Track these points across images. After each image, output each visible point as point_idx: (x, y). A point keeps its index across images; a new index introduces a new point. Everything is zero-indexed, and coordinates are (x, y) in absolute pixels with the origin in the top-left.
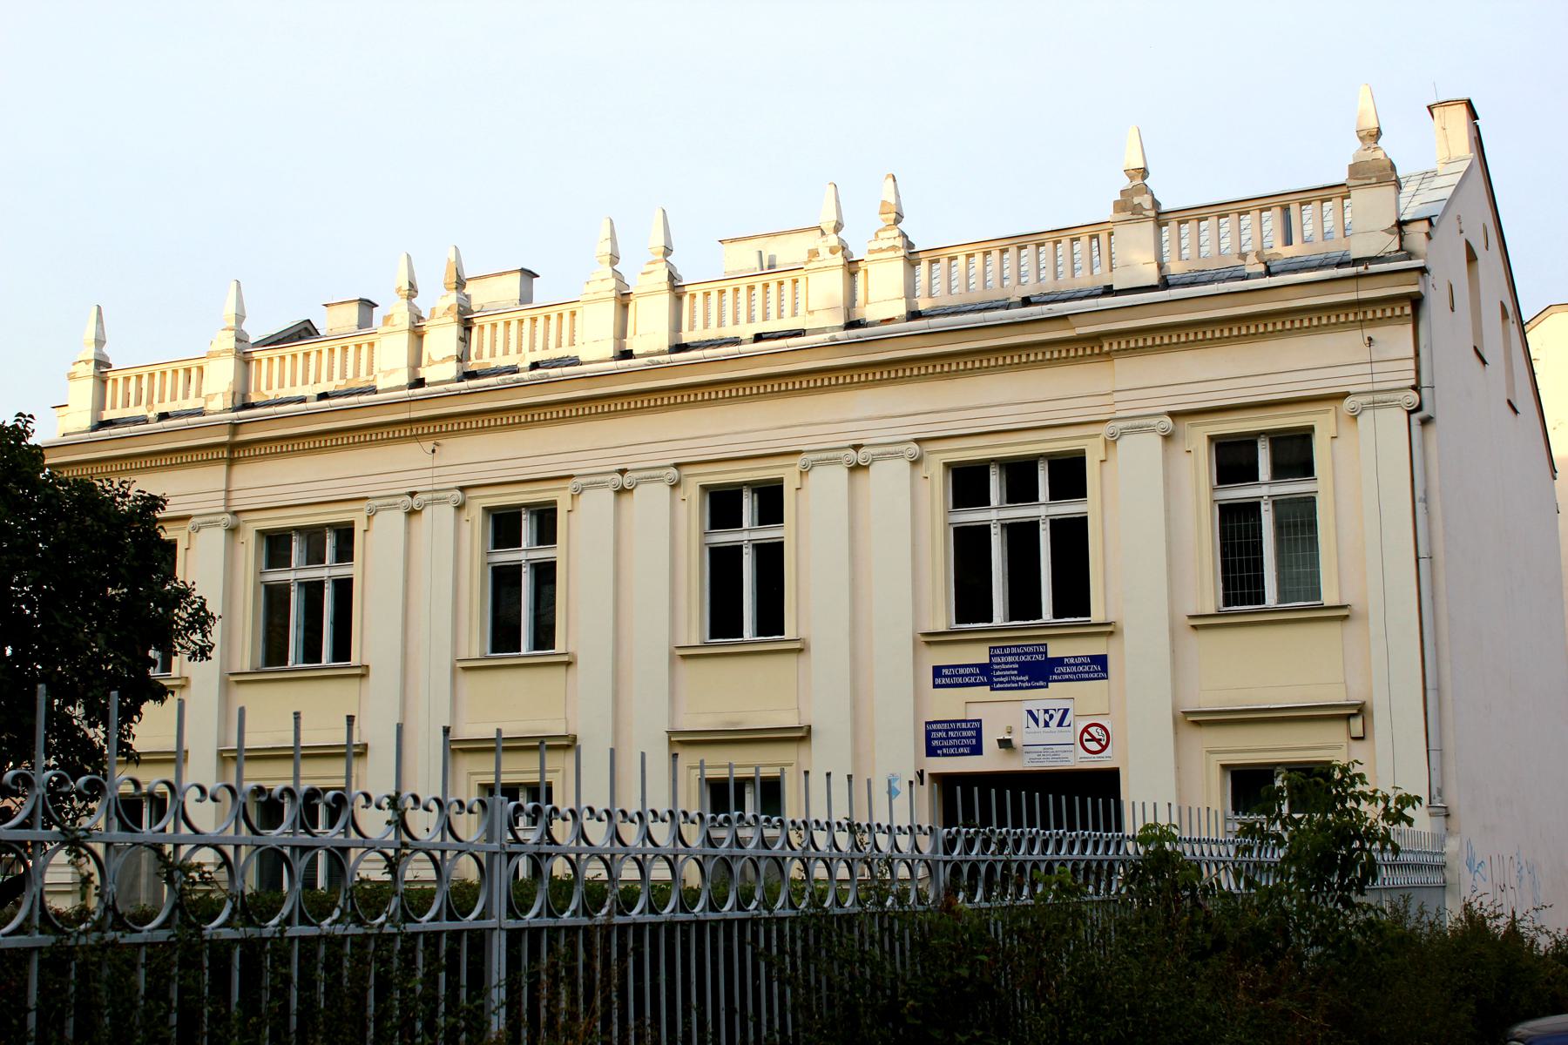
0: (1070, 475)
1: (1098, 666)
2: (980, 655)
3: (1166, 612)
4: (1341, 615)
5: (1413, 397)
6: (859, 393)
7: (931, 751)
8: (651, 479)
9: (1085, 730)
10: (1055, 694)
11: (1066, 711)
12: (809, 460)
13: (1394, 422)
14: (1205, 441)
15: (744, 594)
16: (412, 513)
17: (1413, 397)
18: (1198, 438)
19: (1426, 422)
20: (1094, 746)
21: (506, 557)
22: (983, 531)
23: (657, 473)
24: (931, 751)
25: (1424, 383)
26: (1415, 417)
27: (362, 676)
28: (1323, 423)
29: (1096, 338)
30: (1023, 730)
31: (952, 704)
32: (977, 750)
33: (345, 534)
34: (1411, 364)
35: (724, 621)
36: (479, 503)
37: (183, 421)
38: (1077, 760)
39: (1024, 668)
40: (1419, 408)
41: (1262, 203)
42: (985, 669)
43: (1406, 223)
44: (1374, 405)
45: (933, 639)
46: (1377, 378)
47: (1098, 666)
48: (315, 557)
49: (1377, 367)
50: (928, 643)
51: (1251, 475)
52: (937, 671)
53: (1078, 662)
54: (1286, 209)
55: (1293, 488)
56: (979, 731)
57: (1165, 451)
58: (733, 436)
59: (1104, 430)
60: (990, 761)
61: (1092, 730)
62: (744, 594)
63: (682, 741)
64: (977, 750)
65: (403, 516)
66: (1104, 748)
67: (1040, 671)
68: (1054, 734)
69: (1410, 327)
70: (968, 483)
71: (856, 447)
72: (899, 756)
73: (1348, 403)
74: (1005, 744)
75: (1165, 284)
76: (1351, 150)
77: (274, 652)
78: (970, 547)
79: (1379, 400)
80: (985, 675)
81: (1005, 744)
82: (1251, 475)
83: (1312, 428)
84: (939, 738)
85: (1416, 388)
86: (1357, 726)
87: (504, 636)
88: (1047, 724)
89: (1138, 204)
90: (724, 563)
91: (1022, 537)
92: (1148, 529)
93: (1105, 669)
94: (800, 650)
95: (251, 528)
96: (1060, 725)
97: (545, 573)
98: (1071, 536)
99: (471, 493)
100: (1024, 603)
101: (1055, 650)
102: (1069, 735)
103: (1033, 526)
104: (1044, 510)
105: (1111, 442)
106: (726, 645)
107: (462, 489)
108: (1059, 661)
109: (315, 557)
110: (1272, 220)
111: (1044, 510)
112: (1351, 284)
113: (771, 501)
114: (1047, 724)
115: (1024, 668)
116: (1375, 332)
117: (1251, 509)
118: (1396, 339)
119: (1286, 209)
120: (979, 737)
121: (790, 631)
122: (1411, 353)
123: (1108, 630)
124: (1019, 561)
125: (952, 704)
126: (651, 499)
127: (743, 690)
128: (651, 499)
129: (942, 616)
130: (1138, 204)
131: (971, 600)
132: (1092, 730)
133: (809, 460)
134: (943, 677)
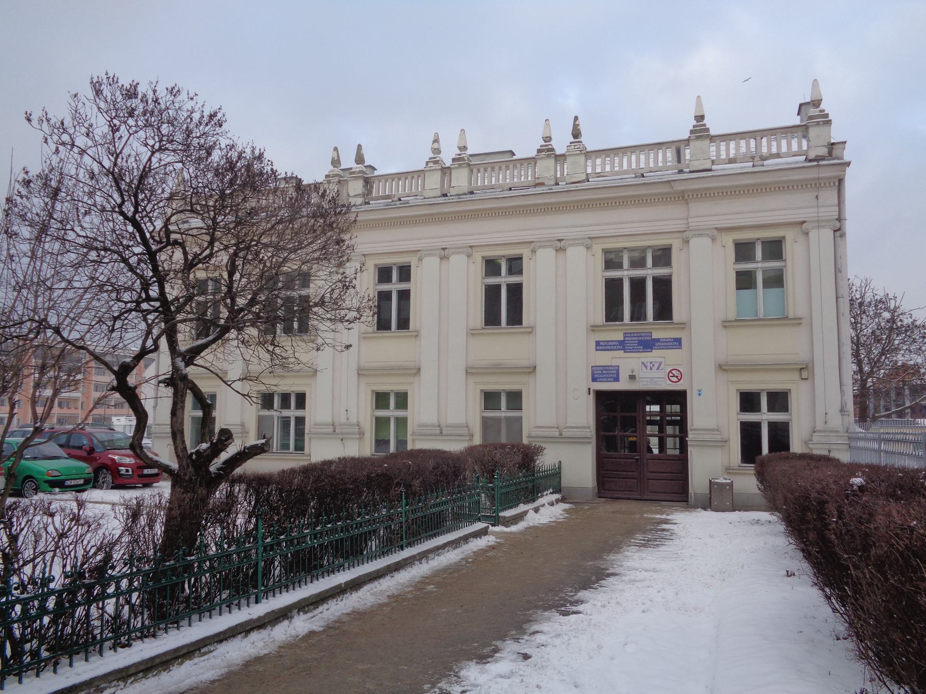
2: (619, 336)
3: (815, 377)
7: (594, 379)
8: (429, 255)
9: (670, 372)
10: (656, 355)
11: (661, 363)
12: (533, 246)
15: (504, 304)
16: (560, 250)
18: (728, 241)
20: (674, 379)
22: (620, 281)
24: (594, 379)
26: (838, 233)
28: (791, 237)
30: (641, 372)
31: (606, 358)
32: (617, 379)
34: (837, 209)
35: (492, 318)
38: (666, 385)
40: (839, 229)
43: (833, 144)
45: (594, 328)
46: (821, 214)
49: (820, 209)
52: (598, 343)
53: (667, 341)
56: (618, 371)
58: (500, 235)
60: (623, 385)
61: (674, 372)
62: (504, 304)
63: (722, 368)
64: (617, 379)
66: (679, 380)
67: (648, 344)
68: (655, 373)
69: (835, 193)
78: (613, 288)
80: (622, 345)
83: (784, 238)
88: (651, 369)
90: (492, 293)
91: (638, 285)
92: (703, 280)
93: (680, 344)
94: (530, 332)
96: (658, 369)
97: (404, 296)
99: (475, 249)
100: (638, 314)
101: (655, 335)
102: (663, 373)
106: (492, 330)
108: (658, 340)
111: (649, 272)
113: (405, 273)
114: (651, 369)
115: (640, 343)
120: (618, 374)
123: (683, 326)
124: (640, 297)
125: (606, 358)
127: (504, 346)
129: (599, 315)
131: (613, 312)
132: (674, 372)
133: (533, 246)
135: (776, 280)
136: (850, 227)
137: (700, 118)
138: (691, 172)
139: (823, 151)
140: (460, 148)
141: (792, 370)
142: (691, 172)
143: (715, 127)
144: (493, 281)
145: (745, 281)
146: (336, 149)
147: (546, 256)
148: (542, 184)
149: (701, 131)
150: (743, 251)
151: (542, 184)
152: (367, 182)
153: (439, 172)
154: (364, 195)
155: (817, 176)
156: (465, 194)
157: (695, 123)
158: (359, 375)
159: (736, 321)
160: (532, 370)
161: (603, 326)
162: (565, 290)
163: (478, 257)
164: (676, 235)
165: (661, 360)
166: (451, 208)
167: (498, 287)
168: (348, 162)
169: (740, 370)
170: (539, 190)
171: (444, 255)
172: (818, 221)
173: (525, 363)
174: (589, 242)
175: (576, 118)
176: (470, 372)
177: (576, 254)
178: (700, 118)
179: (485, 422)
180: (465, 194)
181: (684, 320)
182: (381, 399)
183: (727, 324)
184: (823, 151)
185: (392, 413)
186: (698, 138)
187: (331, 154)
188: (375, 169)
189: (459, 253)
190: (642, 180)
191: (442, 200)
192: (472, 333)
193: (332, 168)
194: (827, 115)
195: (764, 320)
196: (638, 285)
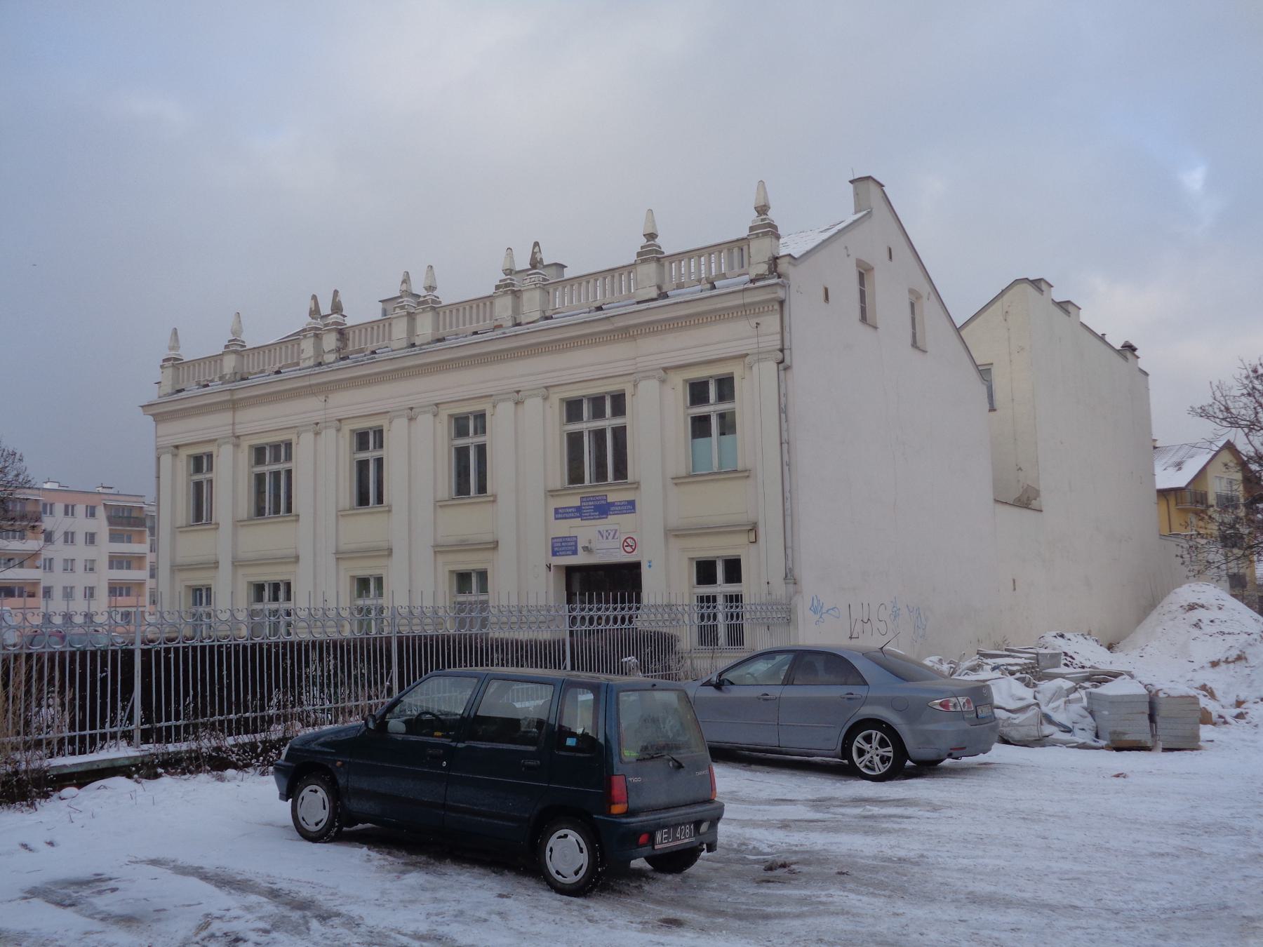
0: (619, 403)
1: (630, 506)
2: (575, 501)
5: (780, 355)
7: (554, 554)
8: (504, 400)
10: (612, 521)
13: (770, 367)
14: (681, 383)
15: (469, 474)
16: (317, 434)
17: (780, 355)
19: (786, 369)
20: (629, 549)
21: (575, 427)
24: (554, 554)
25: (787, 345)
26: (781, 366)
27: (494, 501)
29: (626, 329)
30: (600, 544)
31: (564, 528)
32: (575, 552)
33: (481, 417)
34: (778, 337)
36: (347, 428)
40: (782, 361)
41: (717, 248)
42: (579, 509)
44: (759, 360)
45: (552, 493)
47: (630, 506)
48: (598, 413)
49: (760, 339)
52: (556, 510)
56: (576, 542)
57: (409, 426)
58: (461, 387)
59: (631, 378)
60: (580, 559)
64: (575, 552)
65: (775, 366)
67: (603, 510)
69: (778, 317)
70: (573, 409)
71: (518, 392)
72: (539, 555)
73: (747, 360)
74: (586, 549)
76: (751, 217)
77: (260, 511)
78: (575, 441)
80: (579, 512)
81: (586, 549)
84: (562, 545)
85: (782, 350)
87: (462, 488)
91: (599, 435)
95: (245, 444)
99: (552, 390)
100: (600, 475)
101: (611, 498)
102: (617, 543)
103: (580, 434)
104: (609, 423)
106: (363, 510)
107: (546, 388)
108: (613, 504)
109: (277, 459)
112: (769, 290)
118: (771, 322)
120: (576, 545)
121: (630, 478)
124: (596, 452)
125: (564, 528)
126: (425, 420)
127: (469, 520)
130: (651, 253)
131: (575, 476)
134: (560, 514)
135: (728, 424)
136: (797, 358)
137: (651, 236)
138: (638, 303)
139: (763, 269)
140: (233, 333)
141: (740, 531)
142: (638, 303)
143: (668, 246)
144: (461, 442)
145: (700, 426)
146: (314, 297)
147: (506, 408)
148: (500, 326)
149: (650, 252)
150: (698, 392)
151: (500, 326)
152: (342, 334)
153: (405, 319)
154: (338, 350)
155: (741, 302)
156: (429, 343)
157: (644, 241)
158: (435, 552)
159: (689, 476)
160: (494, 546)
161: (565, 489)
162: (527, 449)
163: (556, 398)
164: (625, 378)
165: (616, 527)
166: (420, 361)
167: (580, 434)
168: (418, 288)
169: (690, 535)
170: (498, 333)
171: (412, 414)
172: (759, 353)
173: (489, 538)
175: (336, 292)
176: (340, 556)
177: (533, 405)
178: (651, 236)
179: (461, 607)
180: (429, 343)
182: (705, 571)
183: (678, 481)
184: (763, 269)
185: (721, 588)
186: (643, 261)
187: (309, 304)
188: (564, 267)
189: (425, 412)
190: (600, 314)
191: (317, 370)
192: (440, 505)
193: (310, 319)
194: (775, 227)
195: (719, 473)
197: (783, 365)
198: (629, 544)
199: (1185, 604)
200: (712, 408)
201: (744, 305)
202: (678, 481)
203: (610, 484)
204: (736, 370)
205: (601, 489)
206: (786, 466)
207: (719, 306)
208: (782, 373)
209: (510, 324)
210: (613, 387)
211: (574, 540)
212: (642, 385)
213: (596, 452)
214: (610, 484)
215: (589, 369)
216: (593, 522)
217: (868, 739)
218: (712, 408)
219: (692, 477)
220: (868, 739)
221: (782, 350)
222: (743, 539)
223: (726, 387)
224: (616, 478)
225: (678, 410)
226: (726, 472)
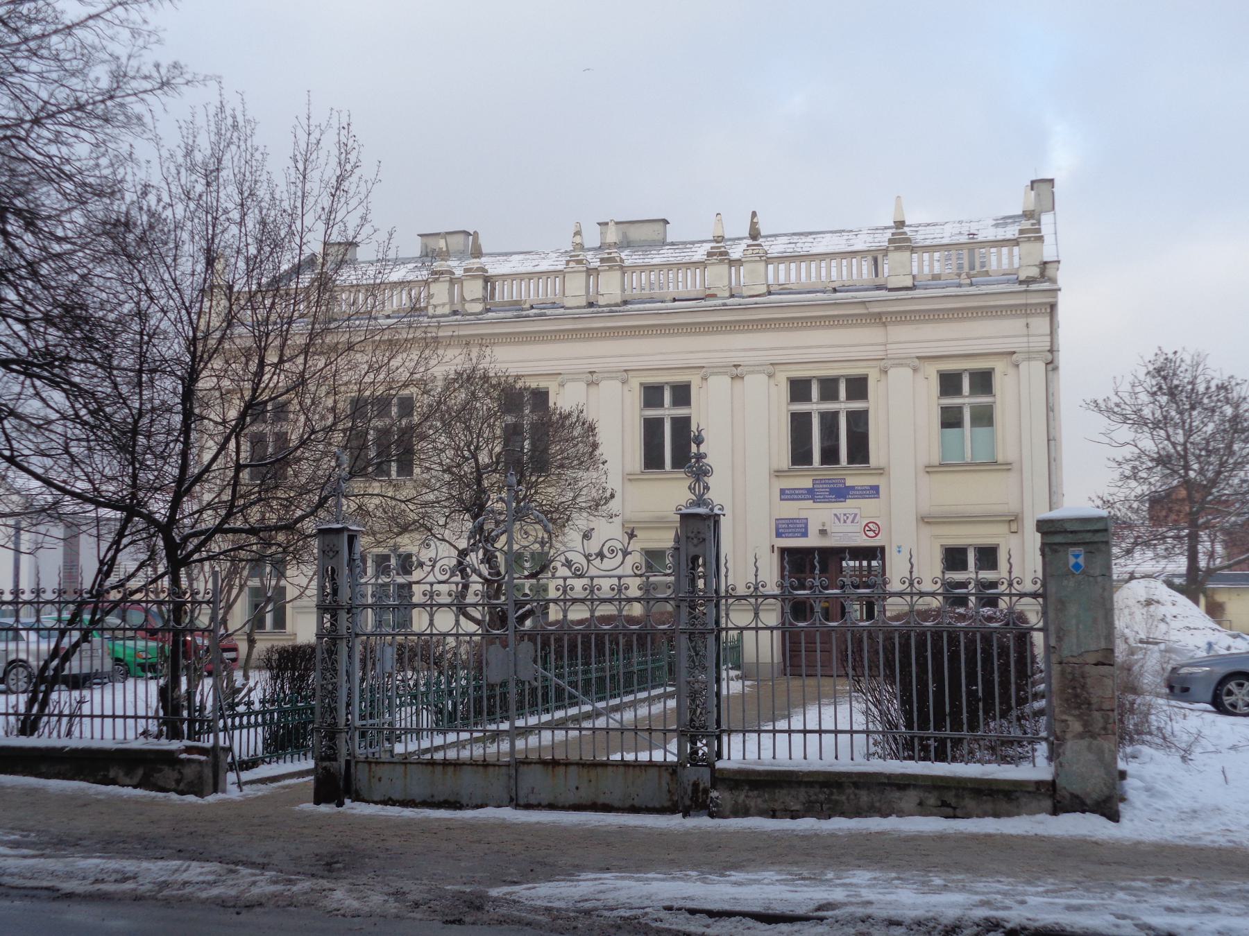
0: (858, 387)
2: (807, 483)
4: (1007, 467)
5: (1049, 357)
6: (849, 330)
7: (779, 535)
10: (850, 505)
12: (705, 372)
13: (1038, 367)
17: (1049, 357)
20: (871, 534)
22: (808, 415)
23: (761, 368)
24: (779, 535)
26: (1050, 367)
29: (879, 315)
30: (830, 524)
31: (792, 510)
32: (805, 534)
34: (1048, 338)
37: (641, 306)
38: (862, 541)
39: (832, 491)
40: (1051, 362)
44: (1029, 359)
45: (778, 474)
47: (874, 491)
49: (1031, 339)
50: (630, 480)
51: (807, 398)
52: (782, 491)
54: (876, 260)
55: (857, 405)
56: (806, 524)
60: (812, 541)
63: (926, 520)
64: (805, 534)
67: (841, 493)
68: (849, 527)
69: (1047, 319)
70: (799, 389)
75: (770, 293)
78: (800, 423)
79: (1030, 355)
80: (811, 494)
82: (807, 398)
86: (1014, 527)
89: (901, 240)
90: (652, 429)
91: (829, 421)
92: (903, 415)
98: (859, 422)
99: (631, 374)
101: (850, 482)
102: (858, 527)
103: (835, 414)
105: (705, 379)
106: (654, 474)
108: (852, 488)
110: (866, 266)
111: (843, 406)
112: (1048, 294)
115: (832, 491)
116: (1030, 320)
117: (659, 422)
118: (1040, 324)
119: (876, 260)
120: (806, 528)
122: (1048, 332)
123: (881, 471)
124: (829, 433)
125: (792, 510)
128: (755, 384)
129: (784, 460)
130: (901, 240)
131: (800, 455)
133: (705, 372)
134: (785, 495)
135: (984, 417)
136: (1063, 358)
145: (951, 419)
147: (720, 384)
150: (949, 383)
151: (714, 296)
155: (1023, 301)
159: (941, 465)
171: (736, 373)
174: (771, 370)
175: (754, 214)
181: (882, 464)
183: (930, 470)
186: (897, 249)
196: (829, 421)
197: (1051, 365)
198: (872, 528)
199: (1142, 599)
200: (966, 400)
201: (1026, 305)
202: (930, 470)
203: (844, 468)
204: (695, 380)
205: (830, 472)
206: (1052, 462)
207: (992, 303)
208: (1050, 374)
209: (727, 294)
210: (855, 371)
211: (805, 522)
212: (712, 379)
213: (829, 433)
214: (844, 468)
215: (827, 350)
216: (829, 505)
217: (1230, 693)
218: (966, 400)
219: (942, 467)
220: (1230, 693)
221: (1051, 351)
222: (1003, 529)
223: (983, 381)
224: (851, 460)
225: (929, 400)
226: (977, 464)
